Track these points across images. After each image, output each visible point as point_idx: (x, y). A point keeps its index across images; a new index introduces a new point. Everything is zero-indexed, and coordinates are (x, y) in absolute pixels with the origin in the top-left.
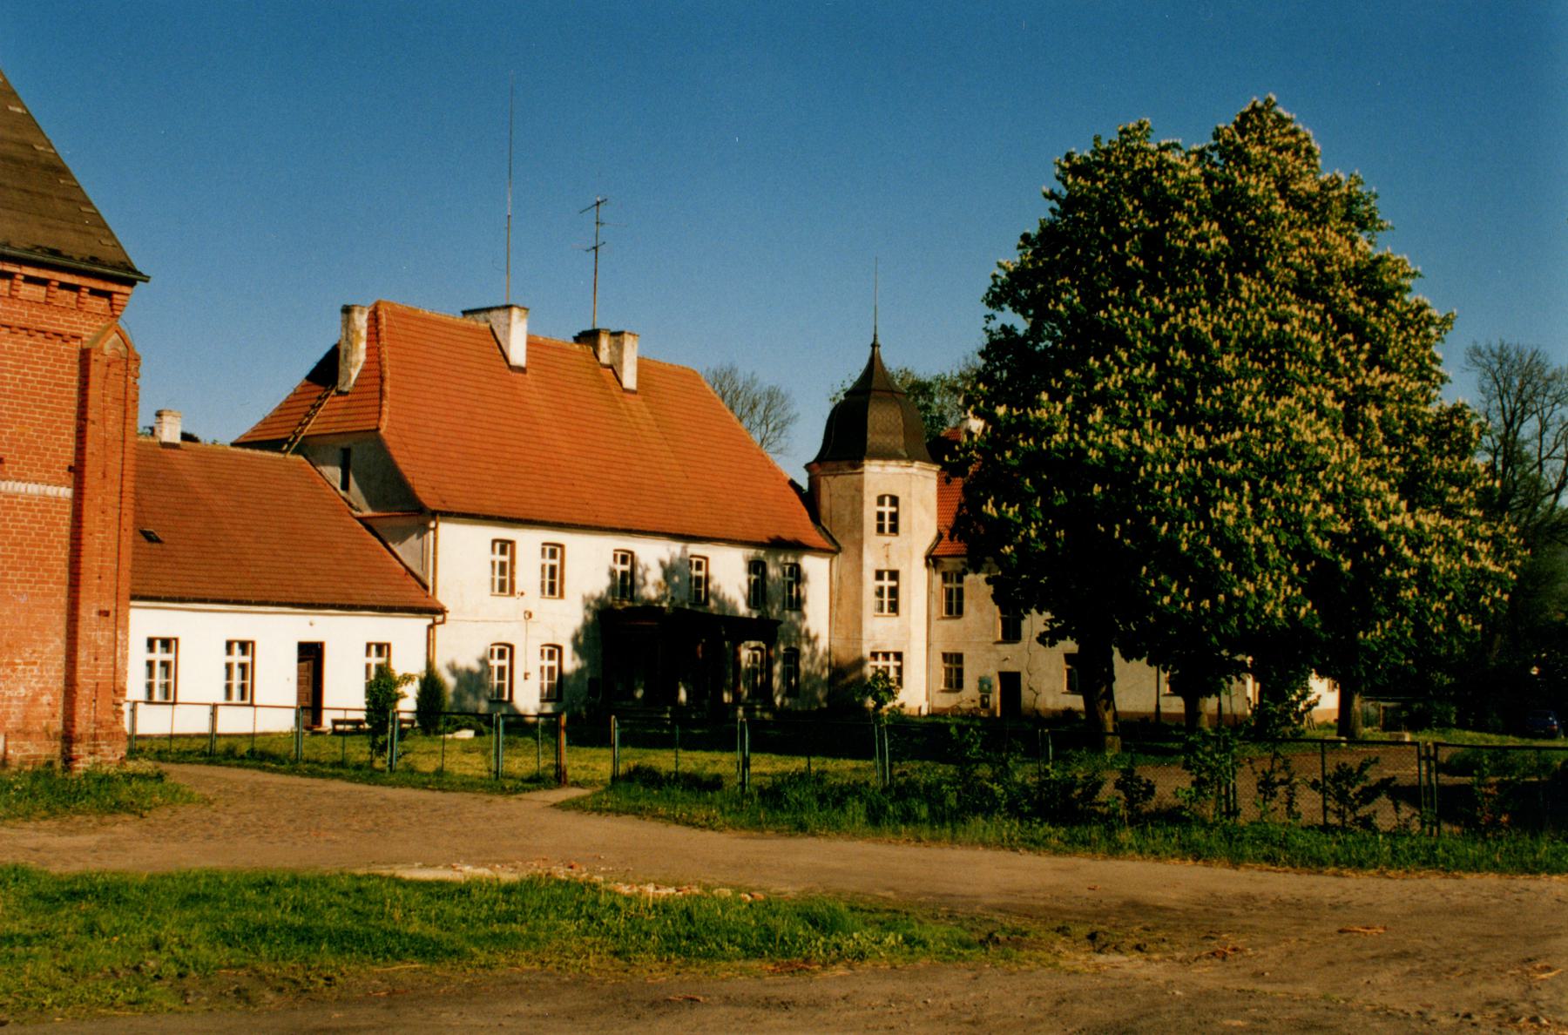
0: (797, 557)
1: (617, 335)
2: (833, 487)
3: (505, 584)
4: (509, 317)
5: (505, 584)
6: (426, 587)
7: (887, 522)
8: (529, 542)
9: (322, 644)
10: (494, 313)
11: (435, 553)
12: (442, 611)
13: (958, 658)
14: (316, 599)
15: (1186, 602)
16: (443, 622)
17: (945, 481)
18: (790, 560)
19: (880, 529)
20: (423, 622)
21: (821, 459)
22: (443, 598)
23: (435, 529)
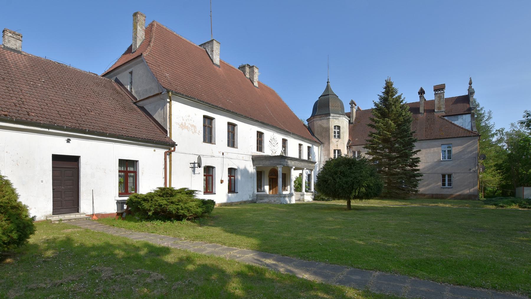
0: (313, 145)
1: (251, 67)
2: (319, 123)
3: (209, 136)
4: (213, 44)
5: (209, 136)
6: (166, 131)
7: (337, 135)
8: (221, 123)
9: (53, 155)
10: (207, 45)
11: (170, 115)
12: (174, 145)
13: (285, 174)
14: (33, 117)
15: (402, 168)
16: (174, 151)
17: (177, 263)
18: (310, 145)
19: (335, 136)
20: (161, 152)
21: (313, 116)
22: (175, 138)
23: (170, 102)
